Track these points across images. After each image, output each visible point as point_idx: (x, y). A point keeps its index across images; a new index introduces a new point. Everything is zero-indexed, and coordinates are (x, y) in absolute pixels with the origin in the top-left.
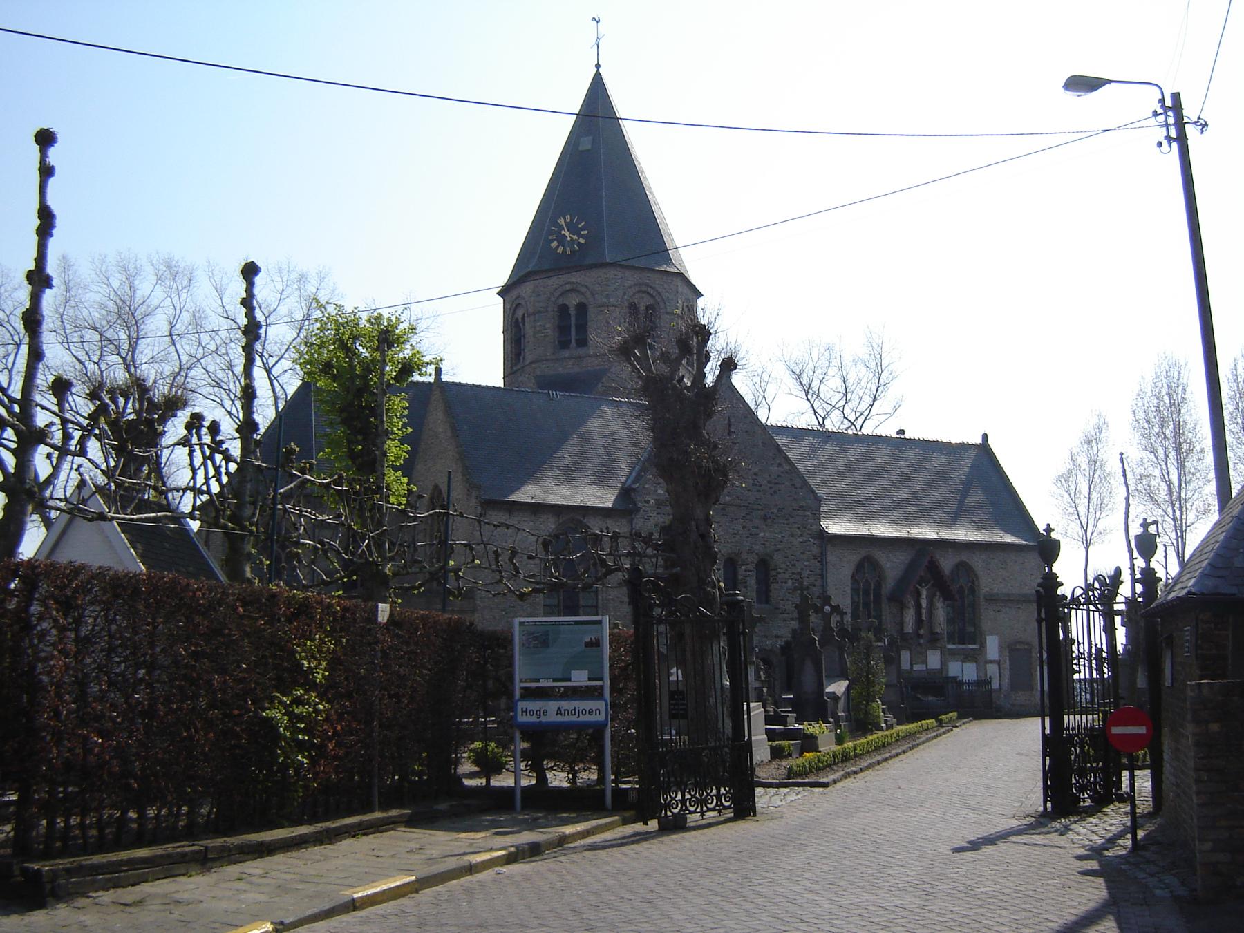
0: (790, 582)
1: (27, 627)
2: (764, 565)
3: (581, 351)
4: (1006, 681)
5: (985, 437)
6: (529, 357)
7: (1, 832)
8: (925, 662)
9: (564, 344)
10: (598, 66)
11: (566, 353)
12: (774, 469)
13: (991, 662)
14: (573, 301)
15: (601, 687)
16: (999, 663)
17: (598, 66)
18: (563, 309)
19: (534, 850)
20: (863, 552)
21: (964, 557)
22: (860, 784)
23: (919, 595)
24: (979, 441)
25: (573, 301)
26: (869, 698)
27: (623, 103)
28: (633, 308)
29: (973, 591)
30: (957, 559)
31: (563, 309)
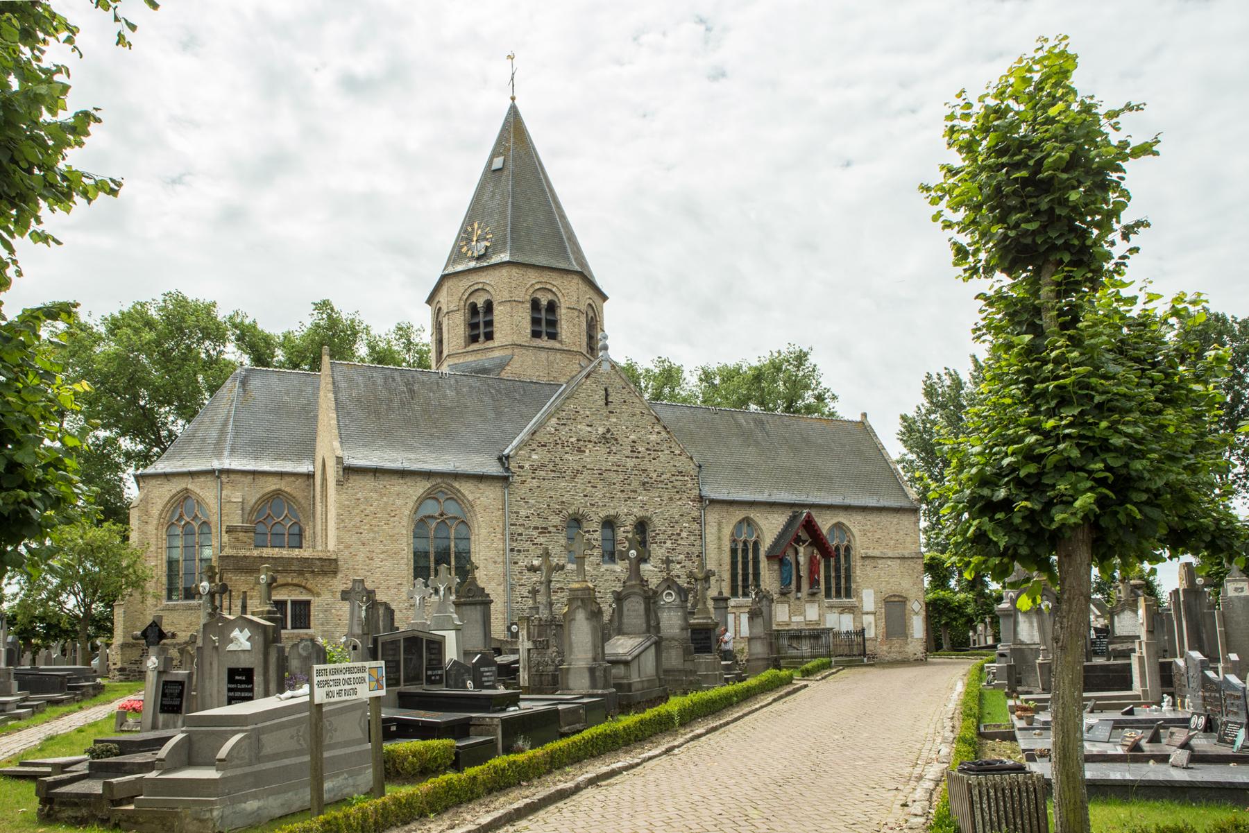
1: (84, 591)
2: (642, 526)
3: (490, 344)
4: (882, 630)
5: (865, 415)
8: (803, 614)
9: (474, 339)
10: (513, 99)
13: (867, 613)
14: (480, 301)
15: (293, 602)
16: (874, 613)
17: (513, 99)
18: (474, 309)
19: (714, 729)
20: (740, 514)
21: (842, 518)
22: (785, 707)
23: (797, 553)
24: (858, 418)
25: (480, 301)
27: (582, 188)
28: (535, 304)
29: (848, 549)
31: (474, 309)
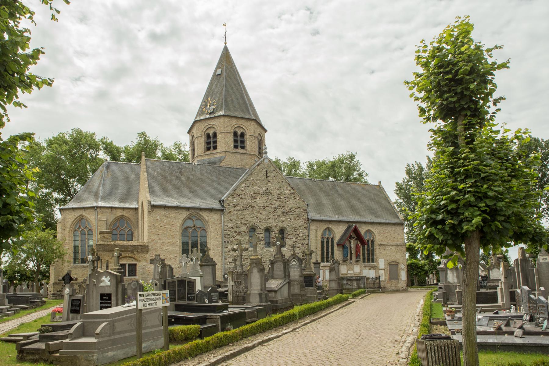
0: (294, 238)
1: (37, 260)
2: (282, 231)
3: (215, 151)
5: (380, 182)
6: (196, 155)
7: (548, 191)
8: (353, 270)
9: (208, 149)
10: (225, 43)
11: (209, 152)
12: (287, 192)
13: (381, 269)
16: (384, 270)
18: (208, 136)
23: (350, 243)
24: (377, 184)
26: (294, 315)
27: (256, 82)
28: (235, 134)
30: (367, 229)
